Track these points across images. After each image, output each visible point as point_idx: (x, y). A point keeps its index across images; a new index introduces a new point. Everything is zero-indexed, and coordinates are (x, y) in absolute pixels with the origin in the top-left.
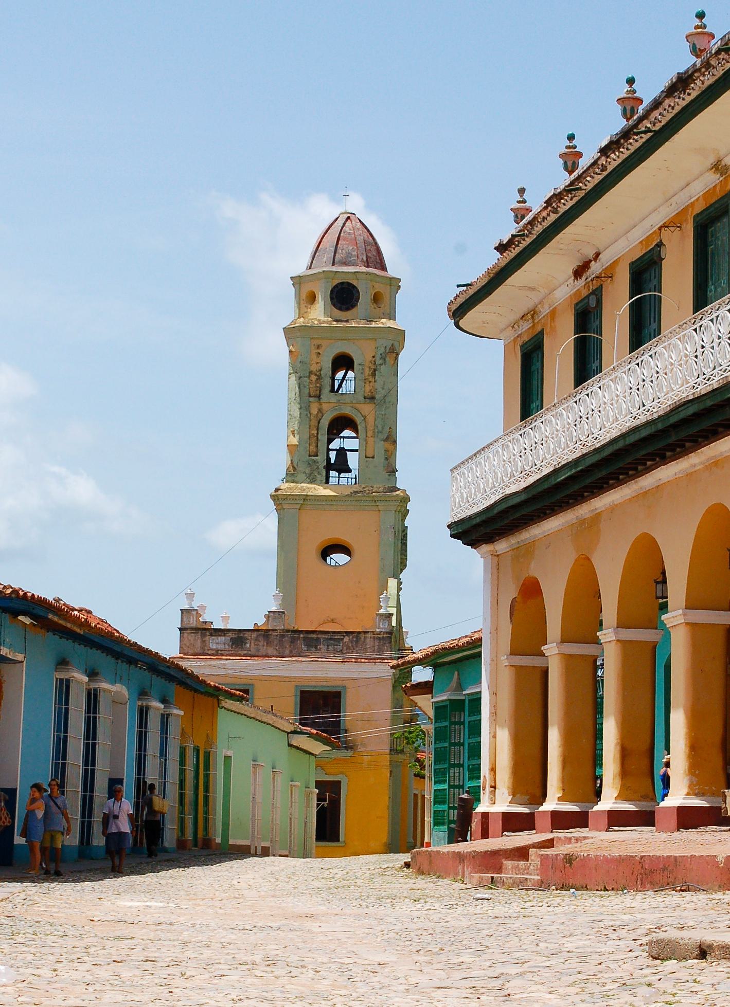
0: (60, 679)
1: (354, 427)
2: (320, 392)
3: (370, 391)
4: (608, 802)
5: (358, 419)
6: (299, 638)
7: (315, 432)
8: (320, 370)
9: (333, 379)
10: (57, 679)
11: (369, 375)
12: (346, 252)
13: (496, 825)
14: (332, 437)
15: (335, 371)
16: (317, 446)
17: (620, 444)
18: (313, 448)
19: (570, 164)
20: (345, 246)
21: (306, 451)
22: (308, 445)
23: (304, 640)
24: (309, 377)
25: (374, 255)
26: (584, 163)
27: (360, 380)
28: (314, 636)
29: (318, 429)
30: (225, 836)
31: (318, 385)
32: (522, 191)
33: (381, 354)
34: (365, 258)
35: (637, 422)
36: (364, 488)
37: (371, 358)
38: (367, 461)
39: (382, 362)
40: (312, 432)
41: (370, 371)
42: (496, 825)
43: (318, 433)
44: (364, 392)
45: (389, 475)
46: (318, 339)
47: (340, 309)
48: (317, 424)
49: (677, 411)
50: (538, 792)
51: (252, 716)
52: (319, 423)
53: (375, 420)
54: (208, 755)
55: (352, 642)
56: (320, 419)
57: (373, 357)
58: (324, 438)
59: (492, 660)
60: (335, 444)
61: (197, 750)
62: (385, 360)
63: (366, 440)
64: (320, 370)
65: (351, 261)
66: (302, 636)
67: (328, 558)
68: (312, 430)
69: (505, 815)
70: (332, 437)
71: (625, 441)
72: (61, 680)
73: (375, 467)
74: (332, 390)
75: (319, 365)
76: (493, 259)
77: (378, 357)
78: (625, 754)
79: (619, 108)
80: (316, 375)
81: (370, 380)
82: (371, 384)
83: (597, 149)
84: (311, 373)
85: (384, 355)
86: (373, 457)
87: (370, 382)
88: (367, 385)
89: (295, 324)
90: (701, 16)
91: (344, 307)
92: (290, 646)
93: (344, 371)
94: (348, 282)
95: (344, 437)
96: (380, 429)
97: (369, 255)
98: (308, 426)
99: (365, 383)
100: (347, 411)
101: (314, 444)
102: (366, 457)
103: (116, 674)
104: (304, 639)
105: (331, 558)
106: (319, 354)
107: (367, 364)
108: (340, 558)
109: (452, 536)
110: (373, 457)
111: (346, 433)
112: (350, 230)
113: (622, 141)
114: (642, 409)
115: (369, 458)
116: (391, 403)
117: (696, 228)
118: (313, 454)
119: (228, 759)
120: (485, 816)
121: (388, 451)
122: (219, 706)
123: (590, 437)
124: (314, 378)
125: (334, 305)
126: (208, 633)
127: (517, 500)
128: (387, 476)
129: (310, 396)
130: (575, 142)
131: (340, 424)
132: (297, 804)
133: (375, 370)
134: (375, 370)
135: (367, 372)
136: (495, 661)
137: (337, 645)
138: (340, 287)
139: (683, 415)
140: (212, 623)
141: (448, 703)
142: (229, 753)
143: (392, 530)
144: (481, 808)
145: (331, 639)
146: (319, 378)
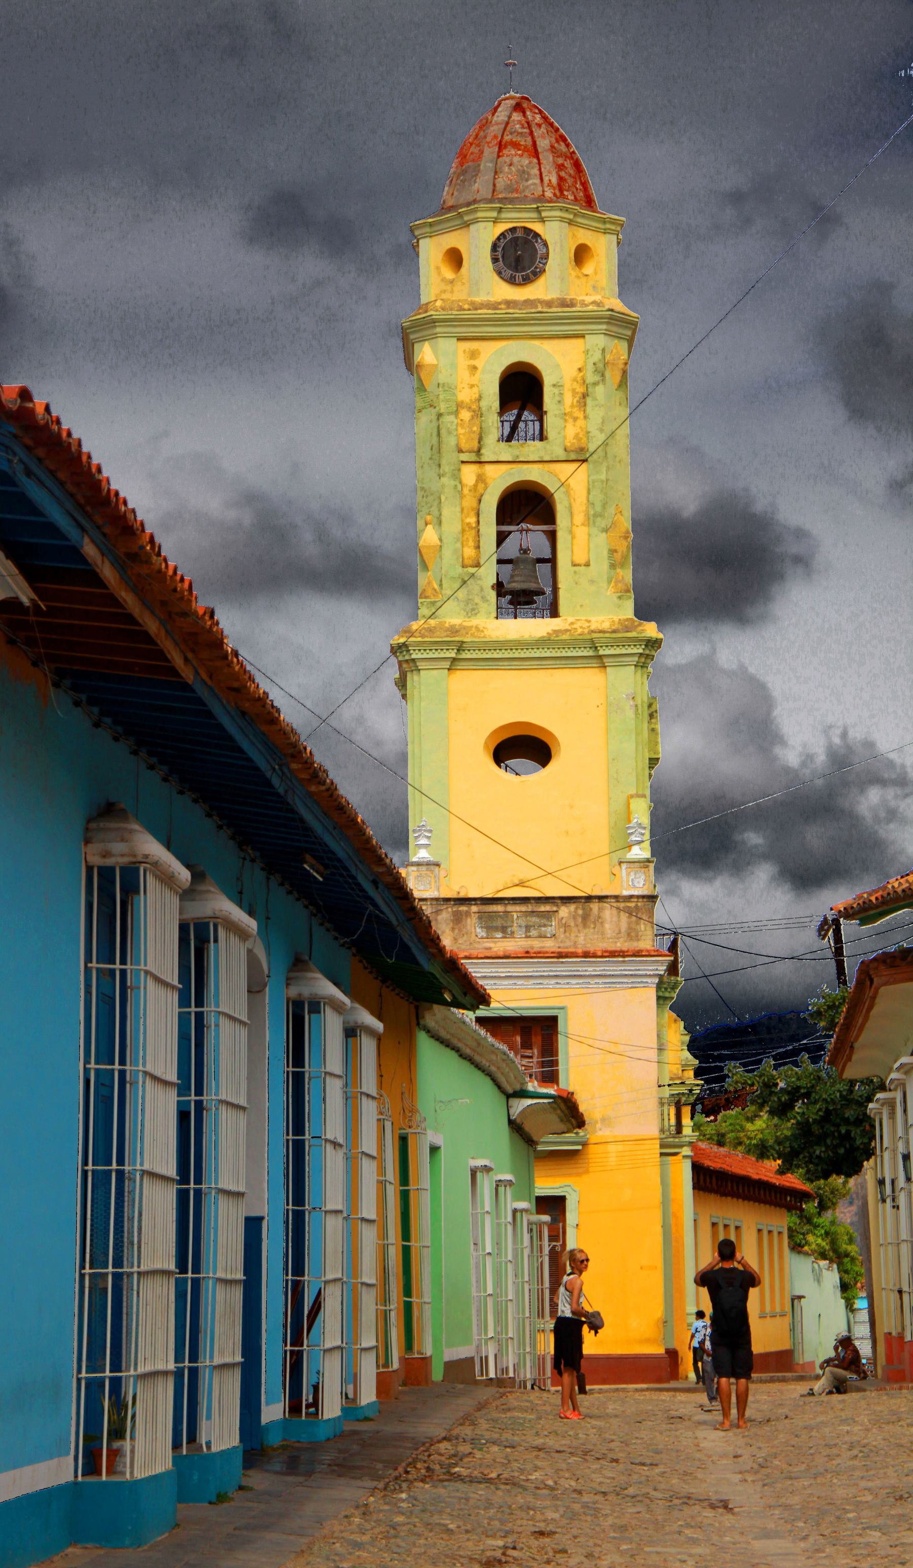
0: (101, 869)
2: (479, 442)
3: (577, 436)
6: (468, 914)
7: (472, 520)
8: (480, 398)
10: (90, 869)
11: (572, 406)
12: (518, 171)
16: (478, 547)
18: (469, 552)
20: (516, 159)
21: (457, 559)
22: (459, 545)
23: (480, 918)
24: (456, 413)
25: (570, 175)
27: (556, 416)
28: (499, 908)
29: (478, 515)
31: (475, 429)
33: (594, 364)
34: (554, 180)
36: (572, 623)
37: (574, 372)
38: (575, 572)
39: (597, 378)
40: (468, 520)
41: (574, 396)
43: (478, 522)
44: (565, 437)
45: (620, 598)
47: (512, 281)
48: (475, 505)
51: (468, 1051)
52: (480, 501)
53: (589, 493)
55: (574, 918)
56: (482, 496)
57: (580, 370)
58: (490, 529)
60: (511, 547)
62: (603, 375)
63: (571, 532)
64: (480, 398)
65: (527, 187)
66: (474, 908)
68: (468, 516)
72: (106, 874)
73: (592, 582)
75: (475, 390)
77: (590, 368)
80: (469, 408)
81: (575, 415)
84: (460, 406)
85: (601, 366)
86: (587, 565)
87: (575, 419)
89: (426, 312)
91: (519, 276)
92: (453, 929)
93: (515, 412)
94: (525, 228)
96: (598, 508)
97: (563, 174)
98: (458, 509)
101: (471, 543)
102: (574, 565)
103: (241, 893)
104: (481, 915)
105: (507, 766)
107: (568, 384)
110: (587, 565)
112: (523, 127)
115: (579, 565)
116: (618, 459)
118: (471, 562)
119: (434, 1149)
121: (616, 551)
122: (418, 1024)
124: (465, 415)
128: (615, 599)
129: (460, 451)
133: (585, 396)
134: (585, 396)
135: (568, 399)
137: (545, 926)
138: (509, 236)
142: (439, 1141)
143: (631, 702)
146: (478, 414)
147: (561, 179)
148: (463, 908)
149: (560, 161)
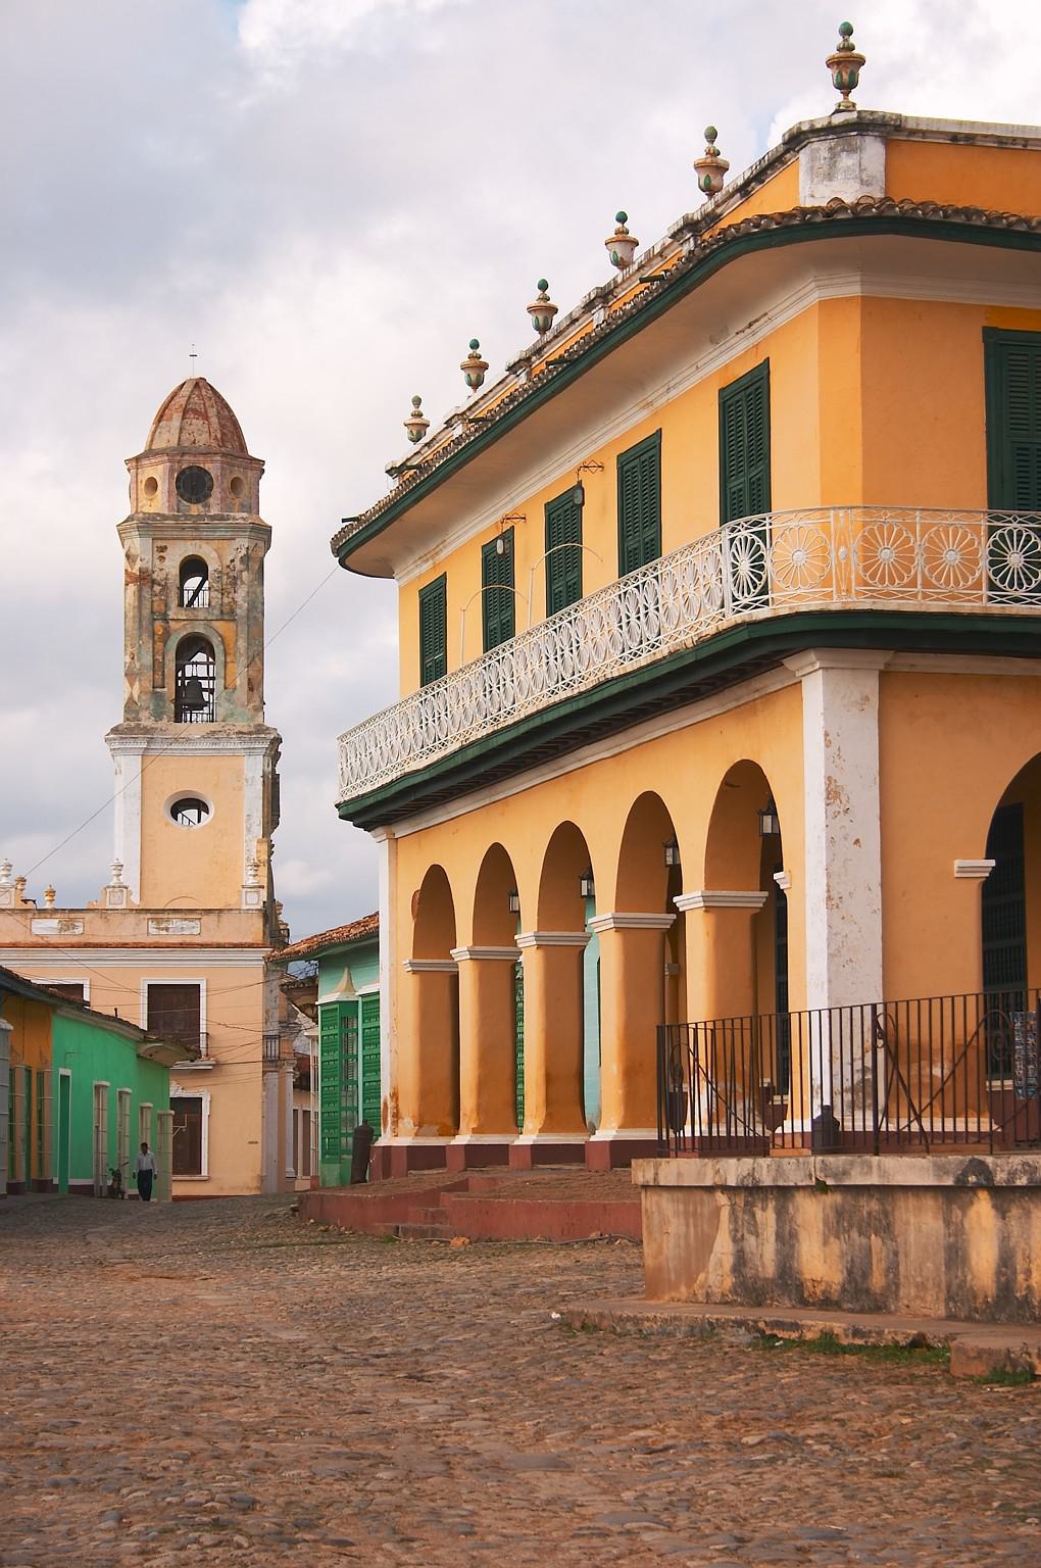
1: (211, 653)
4: (697, 1125)
5: (216, 641)
9: (181, 590)
13: (399, 1163)
14: (181, 662)
15: (183, 580)
17: (537, 722)
18: (158, 677)
19: (473, 377)
26: (491, 378)
30: (63, 1176)
32: (417, 402)
34: (219, 436)
35: (556, 699)
42: (399, 1163)
46: (161, 539)
49: (599, 689)
50: (449, 1122)
54: (41, 1075)
59: (392, 965)
60: (189, 671)
61: (29, 1071)
67: (180, 815)
69: (534, 1147)
70: (181, 662)
71: (542, 719)
74: (181, 604)
76: (387, 487)
78: (550, 1079)
79: (530, 319)
82: (230, 596)
83: (505, 367)
87: (229, 593)
88: (224, 597)
90: (622, 218)
93: (201, 578)
95: (197, 663)
99: (222, 594)
100: (200, 629)
106: (164, 558)
108: (192, 813)
109: (340, 817)
111: (201, 657)
113: (534, 358)
114: (561, 683)
117: (620, 469)
119: (65, 1078)
120: (387, 1149)
123: (502, 711)
125: (182, 496)
126: (30, 915)
127: (418, 779)
130: (478, 351)
131: (193, 644)
132: (127, 1139)
136: (394, 967)
138: (187, 472)
139: (606, 694)
140: (34, 901)
141: (337, 1006)
142: (68, 1072)
144: (382, 1142)
145: (186, 919)
147: (223, 434)
148: (142, 916)
149: (223, 422)
